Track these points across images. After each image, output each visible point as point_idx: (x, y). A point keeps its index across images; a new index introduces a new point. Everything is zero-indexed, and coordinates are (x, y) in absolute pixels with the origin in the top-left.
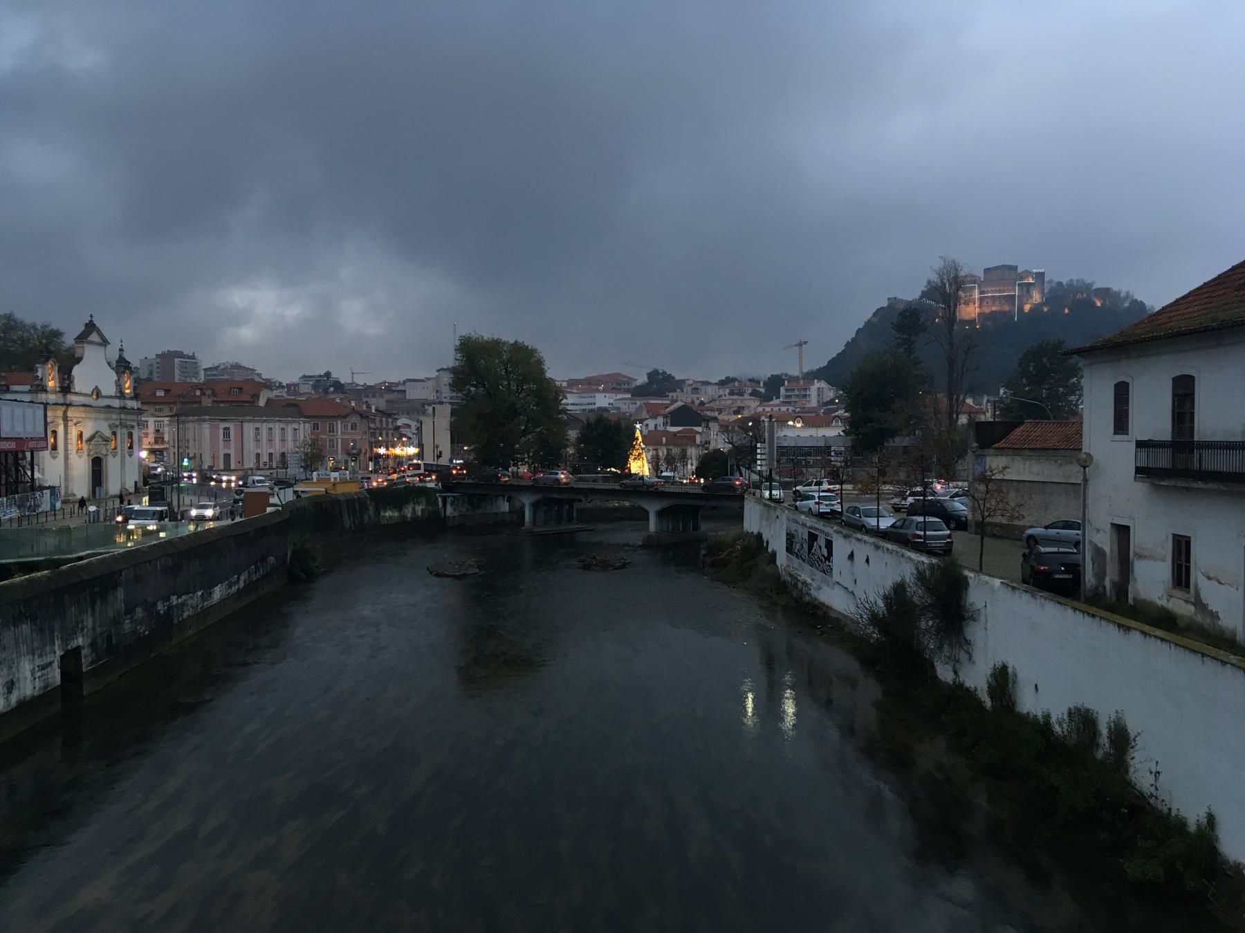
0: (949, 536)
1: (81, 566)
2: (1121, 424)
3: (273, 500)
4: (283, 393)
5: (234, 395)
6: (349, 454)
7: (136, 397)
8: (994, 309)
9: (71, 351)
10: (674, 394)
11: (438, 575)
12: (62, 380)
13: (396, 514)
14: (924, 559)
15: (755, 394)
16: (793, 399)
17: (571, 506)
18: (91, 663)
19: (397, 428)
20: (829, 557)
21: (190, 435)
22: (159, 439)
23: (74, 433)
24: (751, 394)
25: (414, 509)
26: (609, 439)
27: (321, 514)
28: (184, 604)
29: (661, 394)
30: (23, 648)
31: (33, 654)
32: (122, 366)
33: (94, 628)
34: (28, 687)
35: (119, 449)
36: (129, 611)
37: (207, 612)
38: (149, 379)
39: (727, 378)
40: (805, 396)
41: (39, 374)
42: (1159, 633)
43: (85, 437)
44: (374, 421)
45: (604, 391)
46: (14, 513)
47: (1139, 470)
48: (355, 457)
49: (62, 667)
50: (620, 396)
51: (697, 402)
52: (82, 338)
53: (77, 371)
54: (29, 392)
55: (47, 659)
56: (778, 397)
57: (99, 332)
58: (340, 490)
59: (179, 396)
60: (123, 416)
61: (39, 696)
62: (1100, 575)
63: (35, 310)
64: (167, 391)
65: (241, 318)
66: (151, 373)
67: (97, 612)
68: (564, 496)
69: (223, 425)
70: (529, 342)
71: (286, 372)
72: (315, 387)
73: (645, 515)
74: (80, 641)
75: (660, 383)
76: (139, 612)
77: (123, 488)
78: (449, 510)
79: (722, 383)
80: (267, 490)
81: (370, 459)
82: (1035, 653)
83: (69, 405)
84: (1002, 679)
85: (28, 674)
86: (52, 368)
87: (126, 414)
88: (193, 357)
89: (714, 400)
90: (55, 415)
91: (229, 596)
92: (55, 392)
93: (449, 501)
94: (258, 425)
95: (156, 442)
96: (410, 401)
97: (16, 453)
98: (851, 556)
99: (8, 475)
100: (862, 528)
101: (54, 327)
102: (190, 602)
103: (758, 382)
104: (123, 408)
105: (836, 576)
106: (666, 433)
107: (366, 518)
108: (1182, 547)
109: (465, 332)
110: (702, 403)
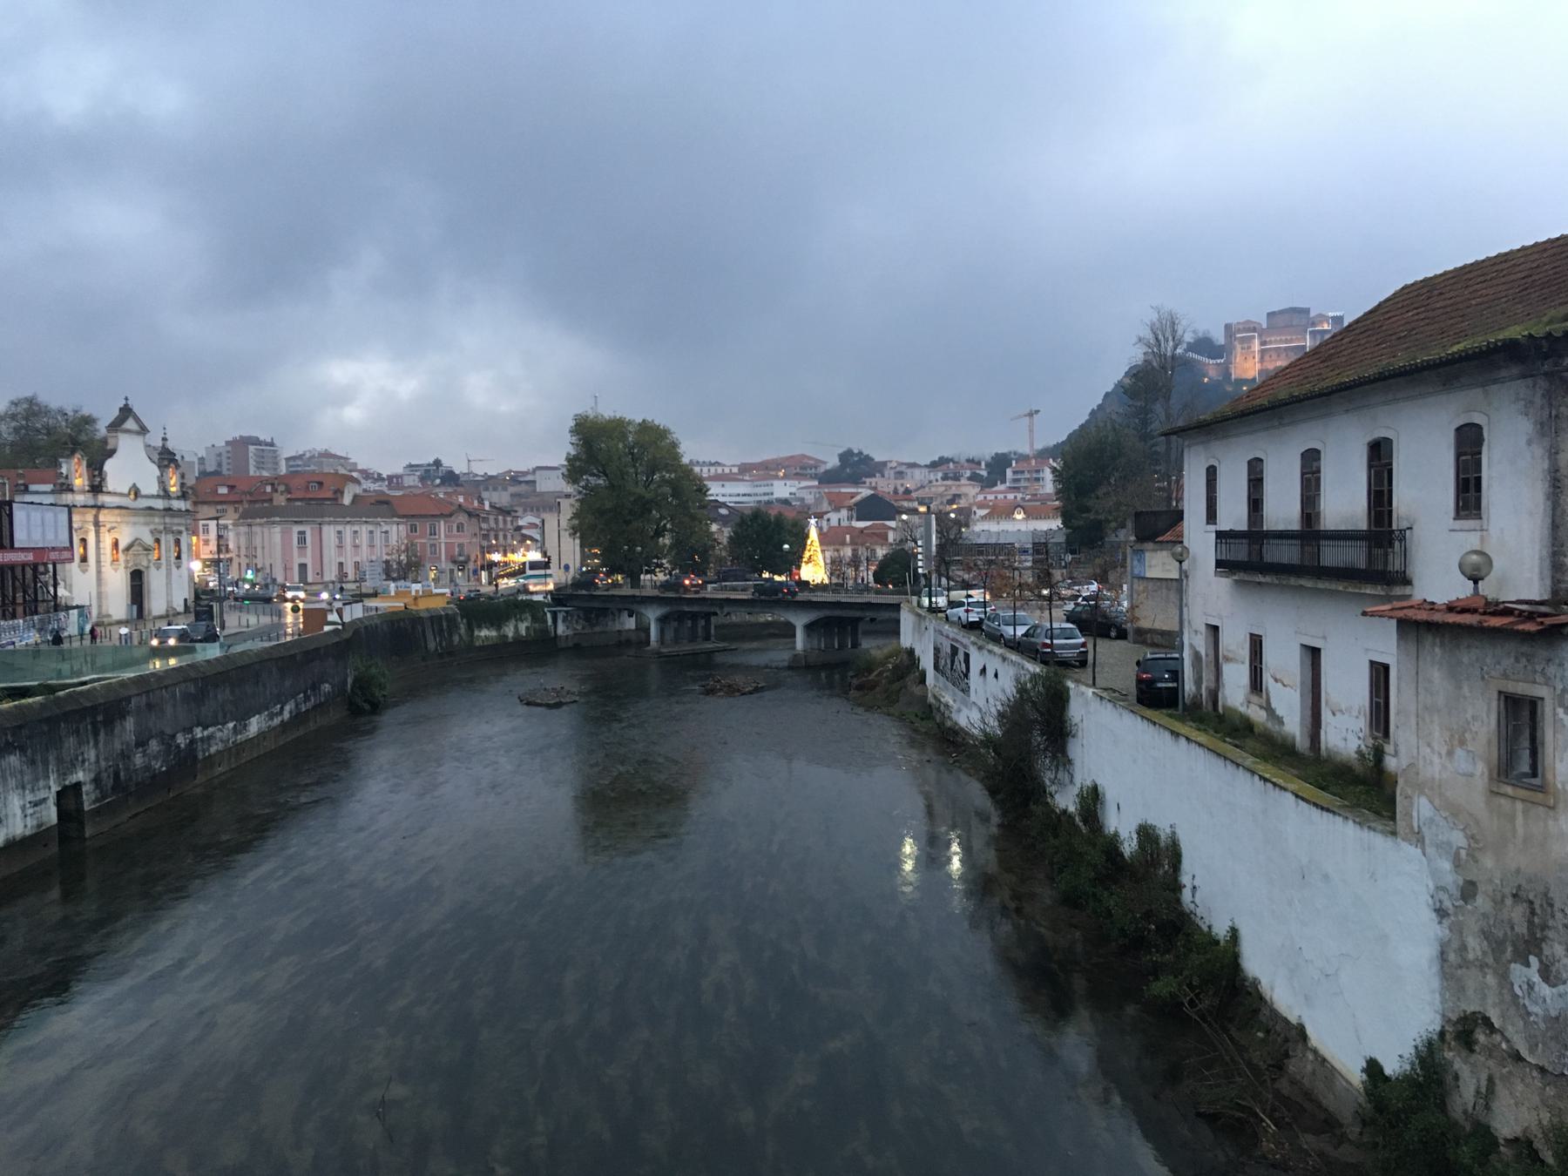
0: (1084, 645)
1: (81, 693)
2: (1211, 516)
3: (333, 617)
4: (382, 487)
5: (319, 492)
6: (454, 562)
7: (183, 496)
8: (1279, 364)
9: (104, 441)
10: (873, 480)
11: (528, 704)
12: (92, 477)
13: (494, 633)
14: (1034, 668)
15: (974, 478)
16: (1023, 484)
17: (708, 622)
18: (94, 802)
19: (519, 528)
20: (966, 675)
21: (258, 541)
22: (222, 546)
23: (107, 541)
24: (970, 479)
25: (516, 627)
26: (769, 537)
27: (400, 636)
28: (210, 737)
29: (856, 480)
30: (12, 782)
31: (24, 788)
32: (166, 458)
33: (97, 761)
34: (19, 825)
35: (163, 561)
36: (141, 743)
37: (239, 748)
38: (217, 473)
39: (941, 459)
40: (1037, 479)
41: (64, 470)
42: (1202, 738)
43: (122, 546)
44: (486, 520)
45: (785, 477)
46: (33, 637)
47: (1219, 564)
48: (462, 565)
49: (58, 804)
50: (804, 484)
51: (901, 490)
52: (116, 426)
53: (109, 466)
54: (53, 492)
55: (42, 794)
56: (1003, 481)
57: (137, 420)
58: (423, 605)
59: (244, 493)
60: (168, 520)
61: (32, 837)
62: (1198, 682)
63: (73, 389)
64: (231, 488)
65: (343, 397)
66: (220, 465)
67: (101, 745)
68: (696, 609)
69: (296, 529)
70: (660, 420)
71: (385, 460)
72: (422, 479)
73: (788, 631)
74: (80, 776)
75: (855, 466)
76: (154, 746)
77: (170, 607)
78: (561, 629)
79: (934, 465)
80: (324, 606)
81: (482, 568)
82: (1127, 769)
83: (100, 507)
84: (1092, 799)
85: (19, 812)
86: (79, 463)
87: (172, 516)
88: (272, 444)
89: (922, 487)
90: (82, 520)
91: (271, 729)
92: (83, 492)
93: (560, 617)
94: (340, 528)
95: (219, 551)
96: (542, 494)
97: (35, 567)
98: (983, 671)
99: (25, 592)
100: (997, 638)
101: (86, 412)
102: (219, 734)
103: (979, 463)
104: (168, 510)
105: (973, 697)
106: (850, 529)
107: (456, 639)
108: (1256, 644)
109: (585, 408)
110: (907, 492)
